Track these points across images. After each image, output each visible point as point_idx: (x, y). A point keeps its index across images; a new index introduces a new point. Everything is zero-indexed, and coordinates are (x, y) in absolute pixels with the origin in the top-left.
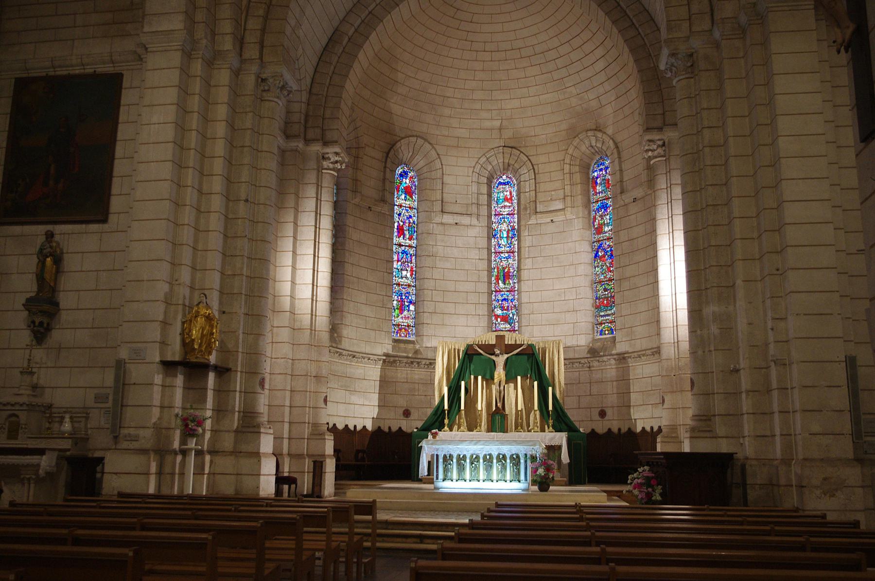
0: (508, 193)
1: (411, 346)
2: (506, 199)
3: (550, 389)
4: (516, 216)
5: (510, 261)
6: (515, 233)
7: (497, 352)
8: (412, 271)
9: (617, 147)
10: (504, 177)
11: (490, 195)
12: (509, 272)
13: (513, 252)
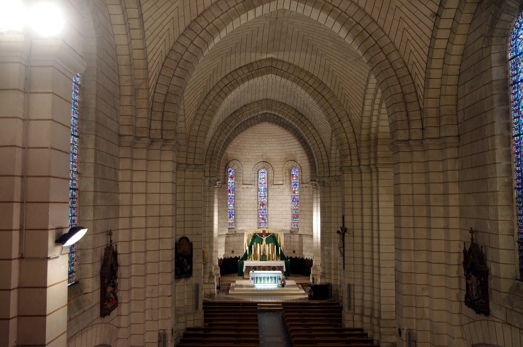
0: (264, 176)
1: (233, 230)
2: (263, 178)
3: (280, 248)
4: (266, 184)
5: (265, 199)
6: (267, 190)
7: (264, 236)
8: (233, 204)
9: (301, 168)
10: (263, 170)
11: (258, 177)
12: (264, 203)
13: (266, 196)
